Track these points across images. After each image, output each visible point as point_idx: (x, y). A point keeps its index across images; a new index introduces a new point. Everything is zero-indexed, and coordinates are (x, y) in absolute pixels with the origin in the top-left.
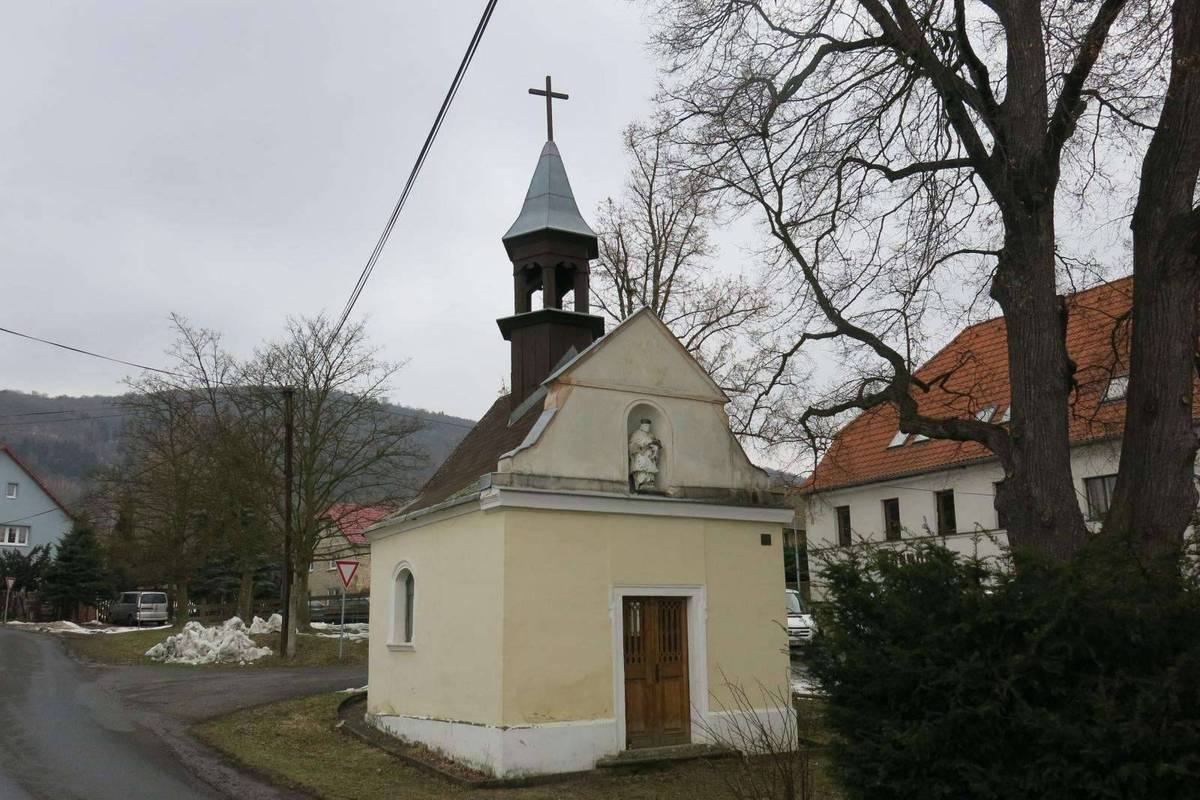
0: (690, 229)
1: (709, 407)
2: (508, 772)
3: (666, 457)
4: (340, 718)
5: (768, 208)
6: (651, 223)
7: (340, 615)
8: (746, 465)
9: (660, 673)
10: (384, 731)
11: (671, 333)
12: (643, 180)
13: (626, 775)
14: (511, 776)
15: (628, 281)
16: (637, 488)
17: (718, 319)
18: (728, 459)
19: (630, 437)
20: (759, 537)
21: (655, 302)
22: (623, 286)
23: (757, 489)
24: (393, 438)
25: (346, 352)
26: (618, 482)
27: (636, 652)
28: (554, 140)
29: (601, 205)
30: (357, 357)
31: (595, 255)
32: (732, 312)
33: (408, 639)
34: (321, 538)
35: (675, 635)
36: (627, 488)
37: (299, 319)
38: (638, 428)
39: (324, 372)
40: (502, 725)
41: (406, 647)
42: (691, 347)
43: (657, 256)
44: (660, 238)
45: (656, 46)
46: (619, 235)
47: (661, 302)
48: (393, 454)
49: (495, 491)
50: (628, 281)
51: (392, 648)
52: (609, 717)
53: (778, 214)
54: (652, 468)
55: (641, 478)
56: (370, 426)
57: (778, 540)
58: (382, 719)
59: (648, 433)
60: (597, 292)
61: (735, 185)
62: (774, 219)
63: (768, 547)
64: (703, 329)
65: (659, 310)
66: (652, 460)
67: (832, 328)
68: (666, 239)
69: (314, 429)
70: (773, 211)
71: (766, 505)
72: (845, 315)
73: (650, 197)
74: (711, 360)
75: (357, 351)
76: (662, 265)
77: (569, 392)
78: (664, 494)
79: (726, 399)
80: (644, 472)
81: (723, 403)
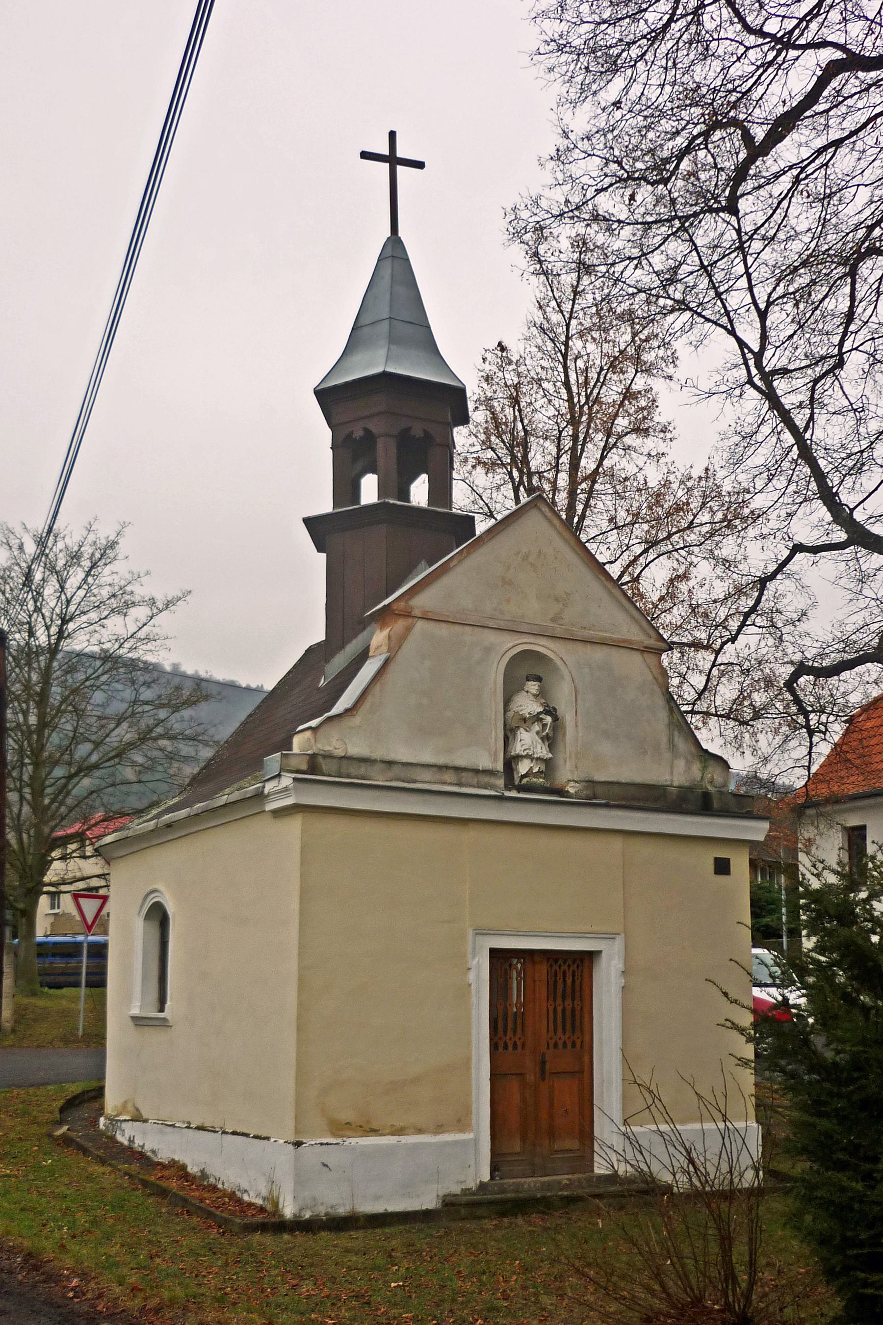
0: (629, 395)
1: (637, 657)
2: (301, 1210)
3: (564, 735)
4: (60, 1123)
5: (741, 344)
6: (567, 384)
7: (80, 974)
8: (693, 749)
9: (548, 1066)
10: (126, 1143)
11: (593, 557)
12: (556, 318)
13: (489, 1217)
14: (307, 1215)
15: (530, 475)
16: (517, 782)
17: (670, 536)
18: (664, 739)
19: (507, 702)
20: (712, 861)
21: (571, 508)
22: (521, 482)
23: (710, 788)
24: (162, 714)
25: (90, 580)
26: (487, 772)
27: (510, 1034)
28: (401, 234)
29: (489, 356)
30: (108, 588)
31: (463, 419)
32: (691, 526)
33: (162, 1010)
34: (53, 860)
35: (573, 1010)
36: (501, 782)
37: (18, 530)
38: (521, 688)
39: (58, 610)
40: (292, 1139)
41: (157, 1019)
42: (626, 578)
43: (575, 437)
44: (581, 407)
45: (553, 60)
46: (515, 401)
47: (580, 508)
48: (161, 736)
49: (287, 780)
50: (530, 475)
51: (139, 1021)
52: (462, 1131)
53: (758, 357)
54: (542, 751)
55: (523, 767)
56: (128, 694)
57: (740, 864)
58: (124, 1125)
59: (536, 696)
60: (480, 491)
61: (691, 309)
62: (751, 363)
63: (727, 877)
64: (646, 551)
65: (576, 520)
66: (542, 739)
67: (840, 536)
68: (590, 409)
69: (42, 698)
70: (751, 351)
71: (725, 813)
72: (858, 516)
73: (566, 344)
74: (655, 598)
75: (109, 580)
76: (583, 450)
77: (408, 630)
78: (561, 792)
79: (663, 646)
80: (530, 757)
81: (659, 652)
